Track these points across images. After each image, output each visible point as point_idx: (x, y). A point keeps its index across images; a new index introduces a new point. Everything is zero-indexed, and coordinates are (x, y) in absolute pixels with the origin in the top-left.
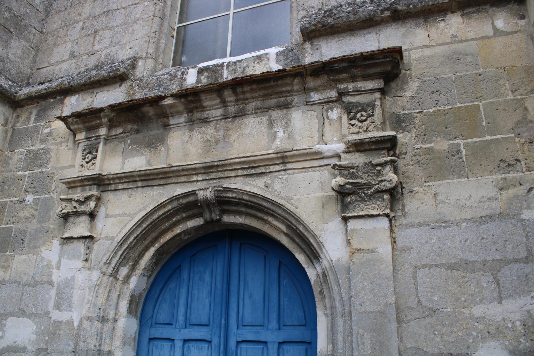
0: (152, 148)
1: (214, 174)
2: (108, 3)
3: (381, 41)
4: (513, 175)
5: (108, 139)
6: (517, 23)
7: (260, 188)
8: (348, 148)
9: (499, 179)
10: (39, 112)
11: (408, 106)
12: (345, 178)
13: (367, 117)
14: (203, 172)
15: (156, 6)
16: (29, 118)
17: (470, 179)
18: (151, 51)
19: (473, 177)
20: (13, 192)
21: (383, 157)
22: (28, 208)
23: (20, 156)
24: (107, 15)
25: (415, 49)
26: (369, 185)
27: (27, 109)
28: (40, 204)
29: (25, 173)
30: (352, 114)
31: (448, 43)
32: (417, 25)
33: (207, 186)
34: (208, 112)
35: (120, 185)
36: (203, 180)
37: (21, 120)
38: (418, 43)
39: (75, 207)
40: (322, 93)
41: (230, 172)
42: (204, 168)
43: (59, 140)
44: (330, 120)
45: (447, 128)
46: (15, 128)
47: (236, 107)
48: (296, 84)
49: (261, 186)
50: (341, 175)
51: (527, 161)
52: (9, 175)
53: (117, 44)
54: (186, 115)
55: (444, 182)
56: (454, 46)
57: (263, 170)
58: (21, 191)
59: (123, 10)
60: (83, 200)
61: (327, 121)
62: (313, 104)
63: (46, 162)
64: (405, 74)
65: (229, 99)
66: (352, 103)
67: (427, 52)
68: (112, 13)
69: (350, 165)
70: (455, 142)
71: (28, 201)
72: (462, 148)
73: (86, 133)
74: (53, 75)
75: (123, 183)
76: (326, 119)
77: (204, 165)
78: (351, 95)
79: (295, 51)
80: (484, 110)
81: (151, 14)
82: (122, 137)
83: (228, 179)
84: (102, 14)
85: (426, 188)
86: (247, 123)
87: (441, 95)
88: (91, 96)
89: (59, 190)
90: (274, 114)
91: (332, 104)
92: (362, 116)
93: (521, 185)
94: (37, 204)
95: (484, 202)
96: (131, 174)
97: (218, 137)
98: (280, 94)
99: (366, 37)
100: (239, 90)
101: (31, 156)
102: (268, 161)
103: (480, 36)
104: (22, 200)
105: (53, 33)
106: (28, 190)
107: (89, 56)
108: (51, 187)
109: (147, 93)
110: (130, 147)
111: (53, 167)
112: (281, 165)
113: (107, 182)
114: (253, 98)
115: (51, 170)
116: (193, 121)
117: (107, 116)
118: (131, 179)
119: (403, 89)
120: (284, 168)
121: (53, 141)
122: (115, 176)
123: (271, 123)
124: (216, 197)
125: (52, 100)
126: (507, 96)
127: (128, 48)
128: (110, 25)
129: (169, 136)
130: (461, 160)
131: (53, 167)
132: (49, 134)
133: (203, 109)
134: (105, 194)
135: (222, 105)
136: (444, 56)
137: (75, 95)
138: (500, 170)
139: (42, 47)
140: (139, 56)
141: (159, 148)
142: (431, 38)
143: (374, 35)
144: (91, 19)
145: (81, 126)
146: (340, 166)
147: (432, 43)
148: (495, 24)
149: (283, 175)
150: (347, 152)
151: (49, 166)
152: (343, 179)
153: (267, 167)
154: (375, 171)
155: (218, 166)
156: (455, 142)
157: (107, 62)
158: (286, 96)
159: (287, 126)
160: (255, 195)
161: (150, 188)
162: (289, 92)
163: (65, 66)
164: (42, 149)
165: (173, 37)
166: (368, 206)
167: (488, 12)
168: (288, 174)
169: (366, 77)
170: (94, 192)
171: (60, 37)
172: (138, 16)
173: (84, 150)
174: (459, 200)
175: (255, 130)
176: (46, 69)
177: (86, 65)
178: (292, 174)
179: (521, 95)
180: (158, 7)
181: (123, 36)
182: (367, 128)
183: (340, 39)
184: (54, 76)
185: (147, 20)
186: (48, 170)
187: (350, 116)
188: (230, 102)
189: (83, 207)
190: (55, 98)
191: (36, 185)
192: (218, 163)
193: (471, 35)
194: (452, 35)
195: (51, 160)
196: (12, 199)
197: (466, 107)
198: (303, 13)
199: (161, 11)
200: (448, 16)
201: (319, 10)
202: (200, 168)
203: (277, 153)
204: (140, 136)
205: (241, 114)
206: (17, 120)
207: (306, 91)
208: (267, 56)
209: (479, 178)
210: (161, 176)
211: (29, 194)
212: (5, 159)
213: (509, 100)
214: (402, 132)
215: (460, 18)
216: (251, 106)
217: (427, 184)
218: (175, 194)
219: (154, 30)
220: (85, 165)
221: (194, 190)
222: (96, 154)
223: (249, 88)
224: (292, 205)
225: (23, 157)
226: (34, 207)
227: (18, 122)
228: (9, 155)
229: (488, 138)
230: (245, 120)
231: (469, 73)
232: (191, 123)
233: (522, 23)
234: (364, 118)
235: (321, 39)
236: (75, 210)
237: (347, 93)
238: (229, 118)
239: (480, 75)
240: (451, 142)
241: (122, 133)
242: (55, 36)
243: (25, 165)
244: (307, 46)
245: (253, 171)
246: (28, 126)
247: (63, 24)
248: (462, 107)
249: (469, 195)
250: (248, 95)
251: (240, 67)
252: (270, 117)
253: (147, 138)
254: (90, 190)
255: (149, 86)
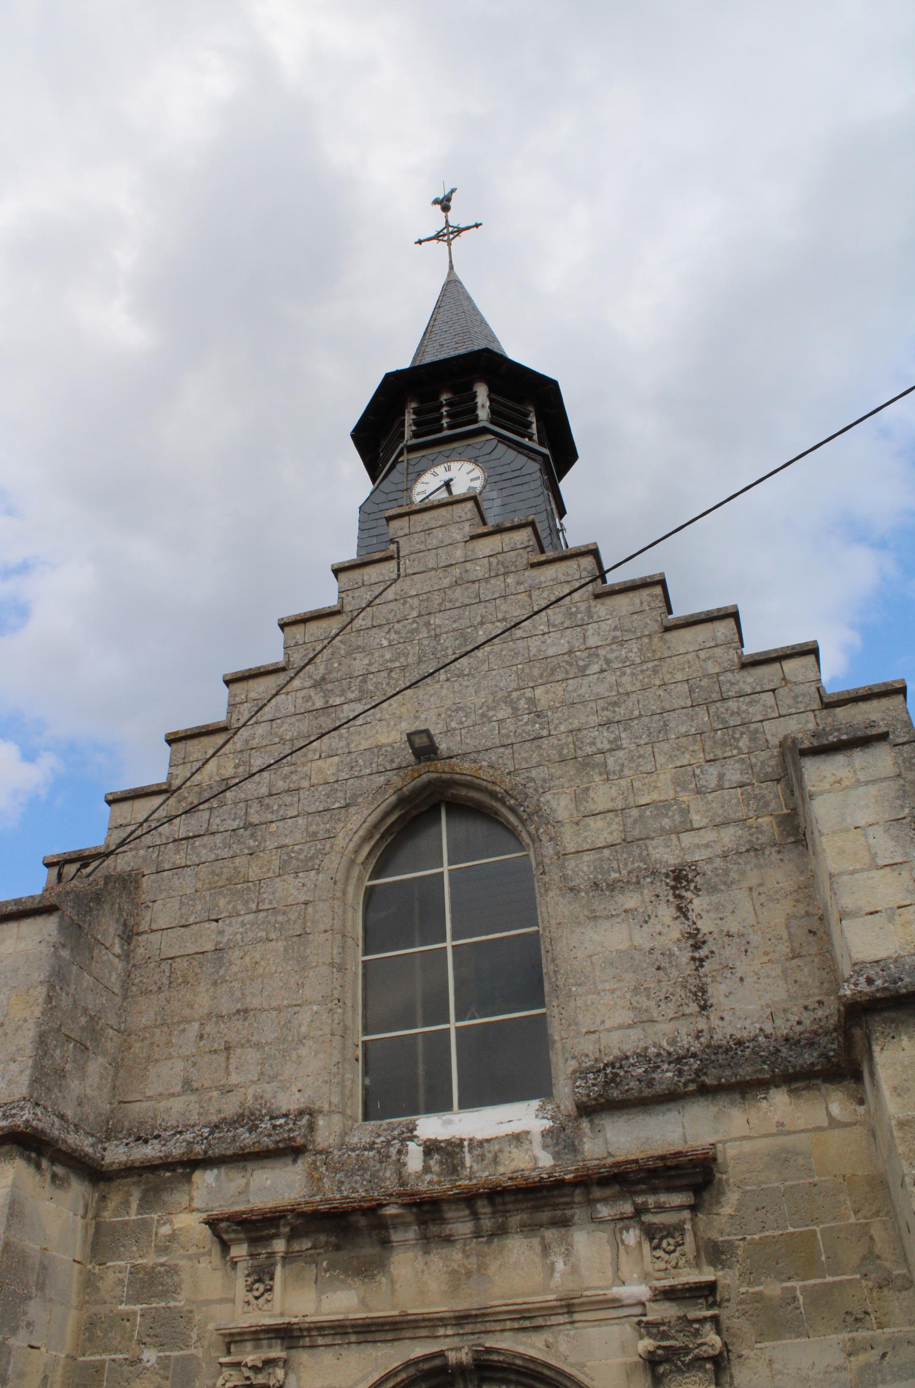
0: (365, 1277)
1: (470, 1326)
2: (243, 994)
3: (686, 1125)
4: (862, 1334)
5: (288, 1258)
6: (855, 1110)
7: (540, 1349)
8: (655, 1295)
9: (846, 1339)
10: (145, 1193)
11: (727, 1230)
12: (655, 1339)
13: (676, 1247)
14: (453, 1322)
15: (333, 1014)
16: (126, 1204)
17: (812, 1339)
18: (335, 1100)
19: (814, 1336)
20: (116, 1343)
21: (700, 1309)
22: (148, 1375)
23: (121, 1276)
24: (245, 1019)
25: (731, 1140)
26: (686, 1350)
27: (120, 1185)
28: (172, 1366)
29: (133, 1307)
30: (656, 1241)
31: (772, 1135)
32: (733, 1103)
33: (461, 1345)
34: (450, 1226)
35: (320, 1338)
36: (454, 1335)
37: (112, 1204)
38: (735, 1133)
39: (248, 1378)
40: (612, 1206)
41: (493, 1324)
42: (456, 1318)
43: (193, 1250)
44: (627, 1247)
45: (777, 1263)
46: (102, 1220)
47: (493, 1220)
48: (578, 1192)
49: (541, 1346)
50: (650, 1335)
51: (878, 1315)
52: (102, 1309)
53: (272, 1079)
54: (416, 1228)
55: (779, 1342)
56: (782, 1140)
57: (540, 1322)
58: (130, 1341)
59: (274, 1013)
60: (260, 1365)
61: (622, 1248)
62: (602, 1222)
63: (173, 1289)
64: (720, 1179)
65: (482, 1210)
66: (654, 1224)
67: (747, 1146)
68: (254, 1015)
69: (659, 1321)
70: (789, 1284)
71: (148, 1361)
72: (798, 1293)
73: (249, 1246)
74: (154, 1118)
75: (324, 1335)
76: (620, 1245)
77: (457, 1314)
78: (652, 1213)
79: (568, 1131)
80: (823, 1239)
81: (327, 1030)
82: (311, 1255)
83: (491, 1335)
84: (234, 1015)
85: (758, 1352)
86: (510, 1246)
87: (769, 1215)
88: (243, 1174)
89: (206, 1343)
90: (550, 1234)
91: (627, 1222)
92: (669, 1244)
93: (872, 1348)
94: (166, 1367)
95: (831, 1373)
96: (341, 1323)
97: (469, 1267)
98: (555, 1206)
99: (666, 1117)
100: (498, 1200)
101: (141, 1276)
102: (549, 1311)
103: (813, 1126)
104: (135, 1359)
105: (140, 1033)
106: (144, 1341)
107: (222, 1093)
108: (190, 1337)
109: (343, 1179)
110: (328, 1274)
111: (188, 1300)
112: (566, 1316)
113: (297, 1333)
114: (517, 1210)
115: (185, 1305)
116: (429, 1238)
117: (289, 1224)
118: (339, 1330)
119: (718, 1202)
120: (571, 1320)
121: (182, 1251)
122: (312, 1325)
123: (546, 1249)
124: (474, 1360)
125: (168, 1174)
126: (848, 1219)
127: (295, 1090)
128: (255, 1039)
129: (392, 1259)
130: (798, 1311)
131: (188, 1300)
132: (173, 1237)
133: (443, 1221)
134: (293, 1352)
135: (472, 1217)
136: (769, 1155)
137: (211, 1170)
138: (847, 1326)
139: (123, 1060)
140: (317, 1107)
141: (378, 1278)
142: (751, 1126)
143: (675, 1113)
144: (215, 1019)
145: (242, 1236)
146: (648, 1323)
147: (752, 1134)
148: (830, 1109)
149: (570, 1330)
150: (654, 1300)
151: (180, 1298)
152: (651, 1341)
153: (547, 1318)
154: (692, 1330)
155: (476, 1316)
156: (789, 1284)
157: (260, 1111)
158: (564, 1209)
159: (568, 1254)
160: (533, 1360)
161: (371, 1344)
162: (566, 1204)
163: (177, 1105)
164: (162, 1265)
165: (357, 1060)
166: (687, 1380)
167: (820, 1090)
168: (577, 1328)
169: (671, 1190)
170: (277, 1352)
171: (158, 1046)
172: (304, 1029)
173: (248, 1275)
174: (799, 1369)
175: (523, 1258)
176: (138, 1104)
177: (219, 1111)
178: (581, 1328)
179: (865, 1218)
180: (336, 1016)
181: (282, 1066)
182: (677, 1264)
183: (631, 1117)
184: (159, 1122)
185: (321, 1040)
186: (178, 1304)
187: (653, 1245)
188: (485, 1214)
189: (260, 1376)
190: (174, 1170)
191: (158, 1331)
192: (478, 1312)
193: (801, 1124)
194: (778, 1122)
195: (183, 1286)
196: (113, 1357)
197: (801, 1233)
198: (573, 1064)
199: (341, 1024)
200: (771, 1091)
201: (596, 1060)
202: (450, 1318)
203: (561, 1300)
204: (342, 1255)
205: (501, 1231)
206: (102, 1204)
207: (591, 1202)
208: (529, 1137)
209: (822, 1338)
210: (388, 1327)
211: (149, 1348)
212: (89, 1279)
213: (852, 1224)
214: (723, 1269)
215: (786, 1095)
216: (515, 1220)
217: (759, 1345)
218: (413, 1356)
219: (335, 1060)
220: (253, 1301)
221: (442, 1351)
222: (271, 1283)
223: (513, 1198)
224: (587, 1375)
225: (125, 1276)
226: (161, 1372)
227: (105, 1208)
228: (97, 1271)
229: (829, 1279)
230: (508, 1241)
231: (801, 1181)
232: (427, 1242)
233: (861, 1110)
234: (672, 1248)
235: (604, 1116)
236: (248, 1382)
237: (647, 1211)
238: (483, 1237)
239: (815, 1185)
240: (785, 1284)
241: (311, 1249)
242: (147, 1042)
243: (131, 1292)
244: (585, 1124)
245: (527, 1324)
246: (127, 1218)
247: (159, 1019)
248: (794, 1233)
249: (811, 1363)
250: (510, 1207)
251: (490, 1152)
252: (543, 1238)
253: (355, 1262)
254: (270, 1346)
255: (345, 1168)
